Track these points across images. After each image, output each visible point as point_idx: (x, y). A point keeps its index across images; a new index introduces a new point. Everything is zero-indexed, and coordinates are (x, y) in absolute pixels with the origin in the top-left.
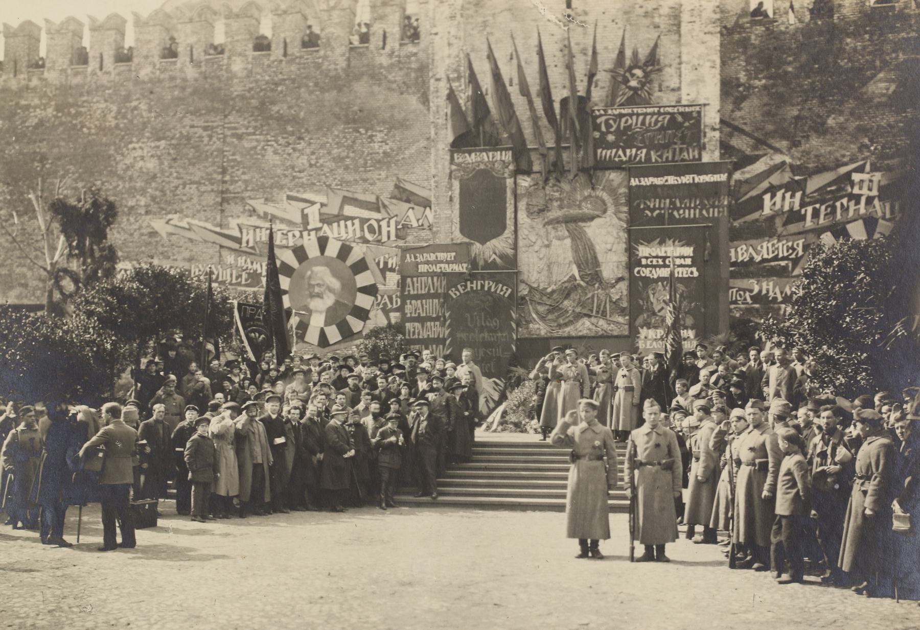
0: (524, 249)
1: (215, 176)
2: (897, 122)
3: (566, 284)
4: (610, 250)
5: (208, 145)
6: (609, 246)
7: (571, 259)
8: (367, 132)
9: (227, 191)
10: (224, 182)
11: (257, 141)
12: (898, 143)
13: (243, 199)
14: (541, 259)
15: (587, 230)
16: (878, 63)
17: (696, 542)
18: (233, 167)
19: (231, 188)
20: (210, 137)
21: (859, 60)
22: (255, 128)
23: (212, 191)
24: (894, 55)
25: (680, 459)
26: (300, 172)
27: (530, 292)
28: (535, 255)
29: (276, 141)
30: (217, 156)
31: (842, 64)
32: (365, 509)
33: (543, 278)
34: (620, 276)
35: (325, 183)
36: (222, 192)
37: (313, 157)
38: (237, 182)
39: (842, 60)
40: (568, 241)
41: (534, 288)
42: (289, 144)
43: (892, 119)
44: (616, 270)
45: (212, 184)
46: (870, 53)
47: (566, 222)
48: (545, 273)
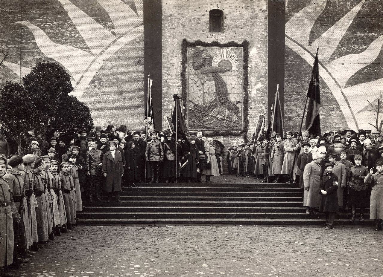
0: (191, 85)
1: (16, 39)
2: (352, 38)
3: (212, 103)
4: (234, 88)
5: (12, 22)
6: (233, 86)
7: (215, 91)
8: (102, 21)
9: (24, 48)
10: (22, 43)
11: (40, 21)
12: (353, 47)
13: (33, 53)
14: (200, 90)
15: (222, 77)
16: (345, 10)
17: (326, 229)
18: (27, 35)
19: (26, 46)
20: (14, 18)
21: (337, 8)
22: (40, 15)
23: (15, 47)
24: (351, 7)
25: (80, 195)
26: (66, 40)
27: (194, 106)
28: (197, 88)
29: (52, 23)
30: (18, 29)
31: (330, 9)
32: (303, 226)
33: (201, 100)
34: (239, 100)
35: (80, 47)
36: (21, 48)
37: (73, 33)
38: (30, 43)
39: (330, 7)
40: (213, 82)
41: (196, 105)
42: (59, 25)
43: (351, 36)
44: (236, 98)
45: (15, 44)
46: (342, 5)
47: (212, 73)
48: (202, 97)
